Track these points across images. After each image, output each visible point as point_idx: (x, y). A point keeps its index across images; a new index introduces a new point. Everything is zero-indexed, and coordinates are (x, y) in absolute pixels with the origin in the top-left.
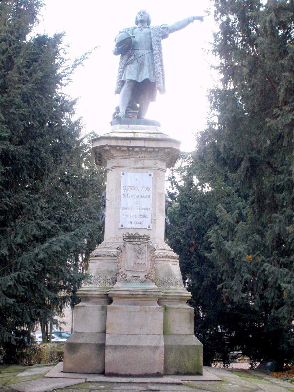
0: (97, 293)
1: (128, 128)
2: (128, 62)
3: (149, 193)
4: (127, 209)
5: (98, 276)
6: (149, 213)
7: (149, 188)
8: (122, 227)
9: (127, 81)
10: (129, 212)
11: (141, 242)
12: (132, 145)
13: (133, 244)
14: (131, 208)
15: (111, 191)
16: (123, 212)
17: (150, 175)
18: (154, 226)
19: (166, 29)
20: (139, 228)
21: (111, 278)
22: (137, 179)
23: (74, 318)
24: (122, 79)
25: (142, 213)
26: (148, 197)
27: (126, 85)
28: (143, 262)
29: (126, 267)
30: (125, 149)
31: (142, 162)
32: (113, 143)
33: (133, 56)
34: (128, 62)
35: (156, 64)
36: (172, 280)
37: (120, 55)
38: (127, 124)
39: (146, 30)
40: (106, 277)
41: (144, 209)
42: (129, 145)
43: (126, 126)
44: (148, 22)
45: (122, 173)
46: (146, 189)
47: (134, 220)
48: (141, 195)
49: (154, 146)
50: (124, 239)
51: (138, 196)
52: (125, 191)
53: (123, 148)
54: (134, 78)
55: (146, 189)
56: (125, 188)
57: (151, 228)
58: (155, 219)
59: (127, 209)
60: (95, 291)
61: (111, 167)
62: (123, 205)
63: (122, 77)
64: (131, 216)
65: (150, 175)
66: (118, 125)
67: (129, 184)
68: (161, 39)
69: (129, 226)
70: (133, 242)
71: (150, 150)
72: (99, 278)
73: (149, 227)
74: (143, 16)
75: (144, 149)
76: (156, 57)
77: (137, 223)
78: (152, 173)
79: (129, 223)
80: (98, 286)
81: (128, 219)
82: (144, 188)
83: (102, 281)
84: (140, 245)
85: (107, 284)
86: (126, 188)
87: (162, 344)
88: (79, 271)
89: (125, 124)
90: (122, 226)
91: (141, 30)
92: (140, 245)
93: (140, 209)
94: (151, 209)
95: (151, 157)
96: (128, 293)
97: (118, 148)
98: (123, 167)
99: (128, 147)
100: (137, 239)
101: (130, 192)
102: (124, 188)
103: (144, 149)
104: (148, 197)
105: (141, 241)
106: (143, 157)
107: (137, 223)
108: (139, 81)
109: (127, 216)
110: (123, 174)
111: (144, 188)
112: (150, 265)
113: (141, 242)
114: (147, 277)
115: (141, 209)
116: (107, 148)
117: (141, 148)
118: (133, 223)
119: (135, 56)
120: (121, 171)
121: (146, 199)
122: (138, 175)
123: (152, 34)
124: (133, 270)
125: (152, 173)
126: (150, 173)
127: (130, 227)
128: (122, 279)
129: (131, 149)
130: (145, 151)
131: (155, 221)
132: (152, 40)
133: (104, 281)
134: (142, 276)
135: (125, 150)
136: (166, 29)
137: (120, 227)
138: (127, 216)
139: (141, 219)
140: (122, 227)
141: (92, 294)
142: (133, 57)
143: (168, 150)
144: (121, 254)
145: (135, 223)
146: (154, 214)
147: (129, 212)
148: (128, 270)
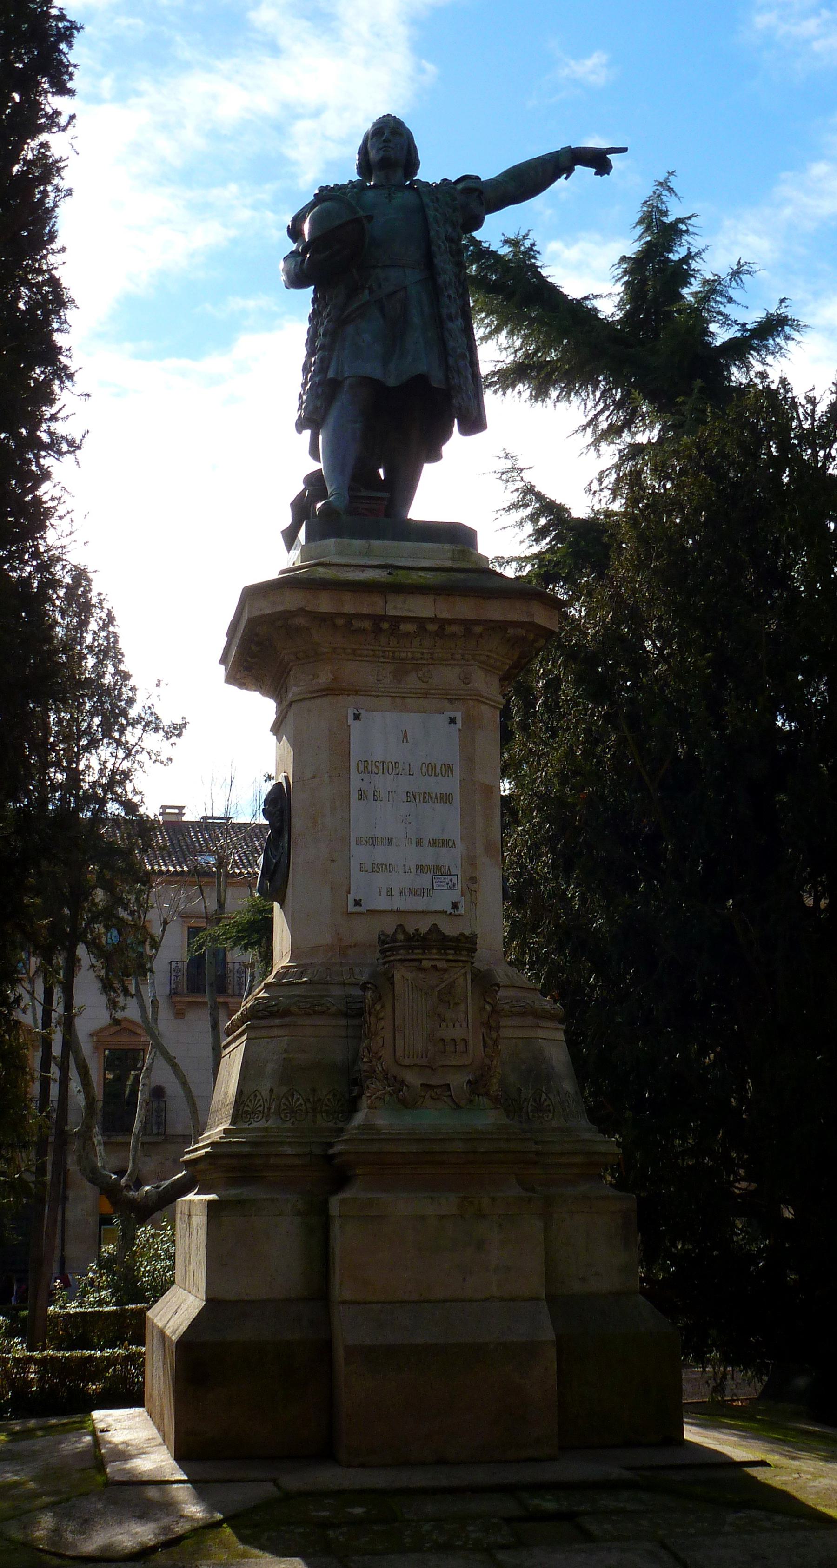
0: (289, 1151)
1: (368, 553)
2: (346, 313)
3: (452, 785)
4: (373, 841)
5: (284, 1089)
6: (451, 858)
7: (448, 769)
8: (358, 909)
9: (347, 382)
10: (381, 854)
11: (448, 961)
12: (391, 612)
13: (421, 969)
14: (390, 841)
15: (314, 777)
16: (359, 854)
17: (452, 721)
18: (472, 902)
19: (476, 194)
20: (420, 909)
21: (334, 1095)
22: (405, 735)
23: (58, 1241)
24: (331, 374)
25: (428, 856)
26: (447, 798)
27: (343, 398)
28: (457, 1033)
29: (399, 1053)
30: (367, 625)
31: (420, 674)
32: (325, 604)
33: (367, 292)
34: (346, 313)
35: (450, 325)
36: (552, 1097)
37: (313, 287)
38: (361, 537)
39: (401, 198)
40: (314, 1090)
41: (435, 843)
42: (380, 612)
43: (357, 542)
44: (411, 162)
45: (351, 712)
46: (438, 771)
47: (400, 881)
48: (422, 791)
49: (471, 615)
50: (382, 951)
51: (411, 797)
52: (366, 776)
53: (357, 624)
54: (372, 369)
55: (438, 771)
56: (365, 767)
57: (462, 910)
58: (473, 880)
59: (373, 841)
60: (281, 1143)
61: (311, 692)
62: (358, 829)
63: (328, 367)
64: (391, 868)
65: (452, 721)
66: (331, 541)
67: (378, 756)
68: (459, 230)
69: (382, 903)
70: (420, 960)
71: (454, 629)
72: (252, 1097)
73: (455, 906)
74: (391, 145)
75: (431, 627)
76: (449, 296)
77: (413, 892)
78: (459, 716)
79: (384, 892)
80: (288, 1125)
81: (381, 880)
82: (430, 769)
83: (303, 1108)
84: (445, 971)
85: (319, 1116)
86: (367, 768)
87: (549, 1335)
88: (707, 1060)
89: (353, 536)
90: (357, 903)
91: (390, 197)
92: (445, 971)
93: (419, 843)
94: (458, 842)
95: (453, 654)
96: (414, 1148)
97: (340, 622)
98: (356, 692)
99: (377, 619)
100: (434, 951)
101: (383, 782)
102: (361, 768)
103: (431, 627)
104: (447, 798)
105: (451, 957)
106: (426, 656)
107: (413, 892)
108: (392, 382)
109: (377, 868)
110: (357, 717)
111: (430, 769)
112: (485, 1045)
113: (448, 961)
114: (477, 1086)
115: (426, 843)
116: (301, 621)
117: (421, 622)
118: (396, 892)
119: (371, 292)
120: (348, 705)
121: (438, 806)
122: (412, 721)
123: (431, 213)
124: (424, 1061)
125: (459, 716)
126: (452, 714)
127: (388, 908)
128: (387, 1098)
129: (385, 626)
130: (440, 634)
131: (474, 887)
132: (432, 233)
133: (309, 1105)
134: (458, 1081)
135: (364, 630)
136: (476, 194)
137: (352, 908)
138: (377, 868)
139: (425, 880)
140: (358, 909)
141: (268, 1156)
142: (365, 296)
143: (521, 632)
144: (378, 1007)
145: (402, 893)
146: (471, 861)
147: (381, 854)
148: (407, 1062)
